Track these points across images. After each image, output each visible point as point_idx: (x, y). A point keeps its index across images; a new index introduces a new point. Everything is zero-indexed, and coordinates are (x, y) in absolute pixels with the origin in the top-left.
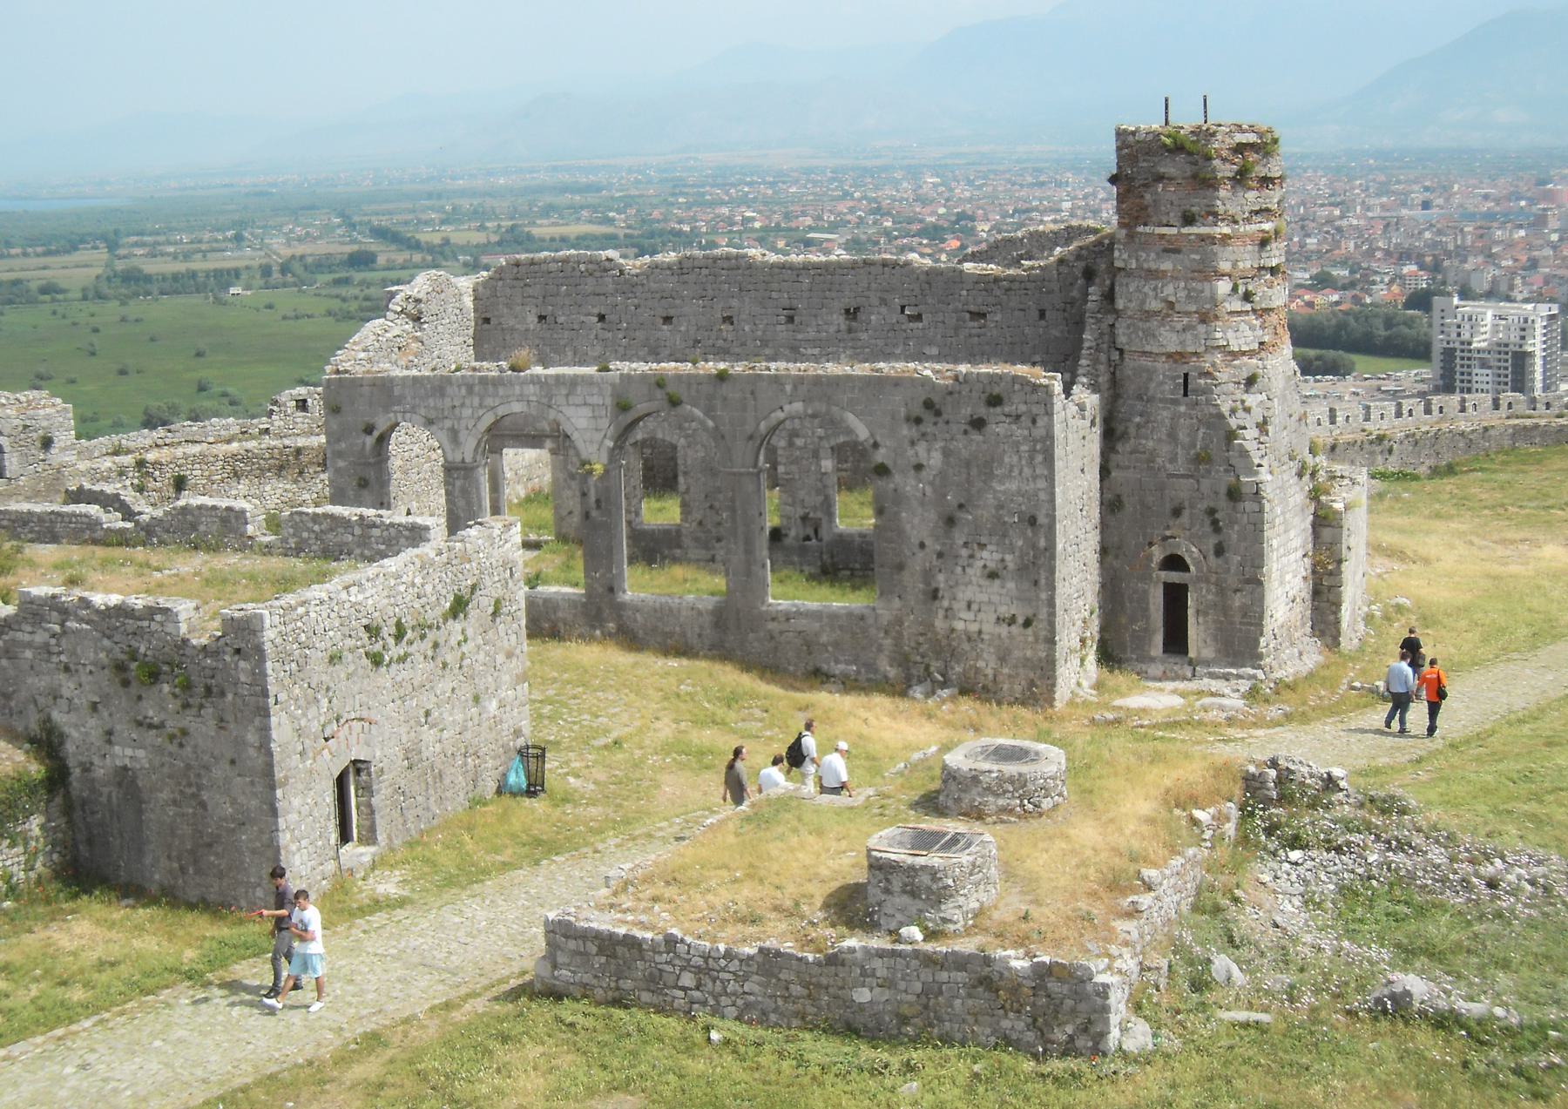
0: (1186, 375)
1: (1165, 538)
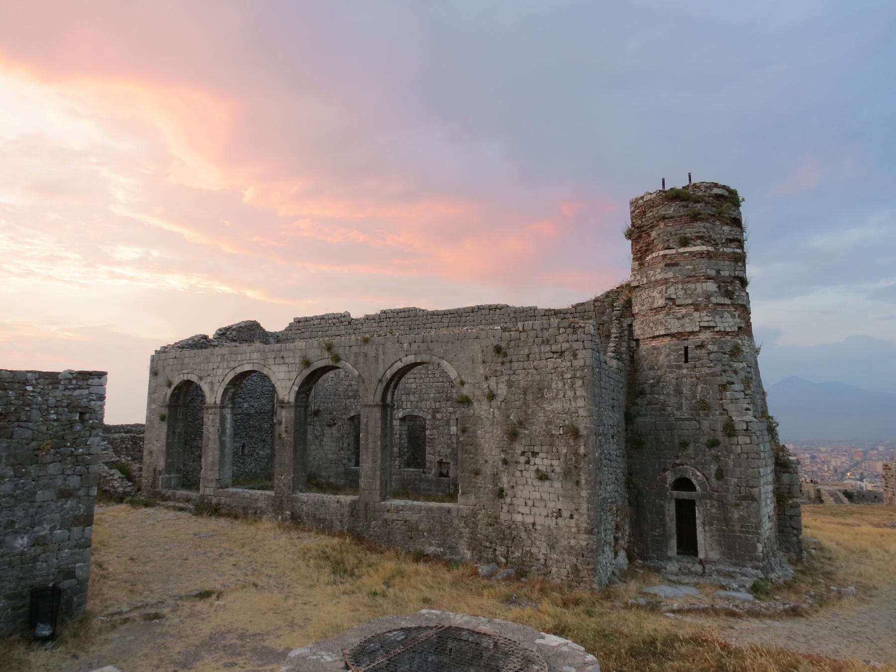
0: (686, 348)
1: (675, 465)
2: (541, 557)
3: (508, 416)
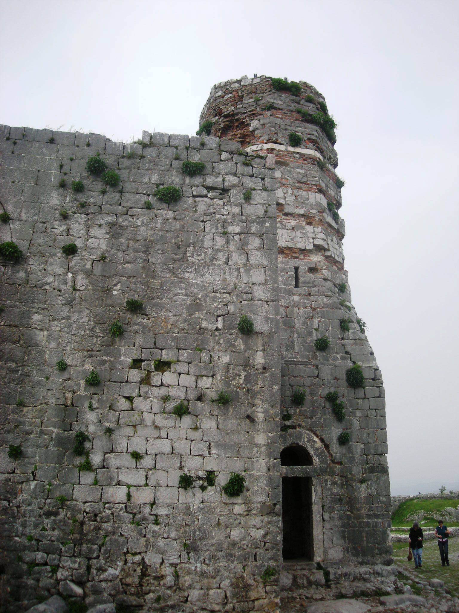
2: (167, 570)
3: (108, 290)
